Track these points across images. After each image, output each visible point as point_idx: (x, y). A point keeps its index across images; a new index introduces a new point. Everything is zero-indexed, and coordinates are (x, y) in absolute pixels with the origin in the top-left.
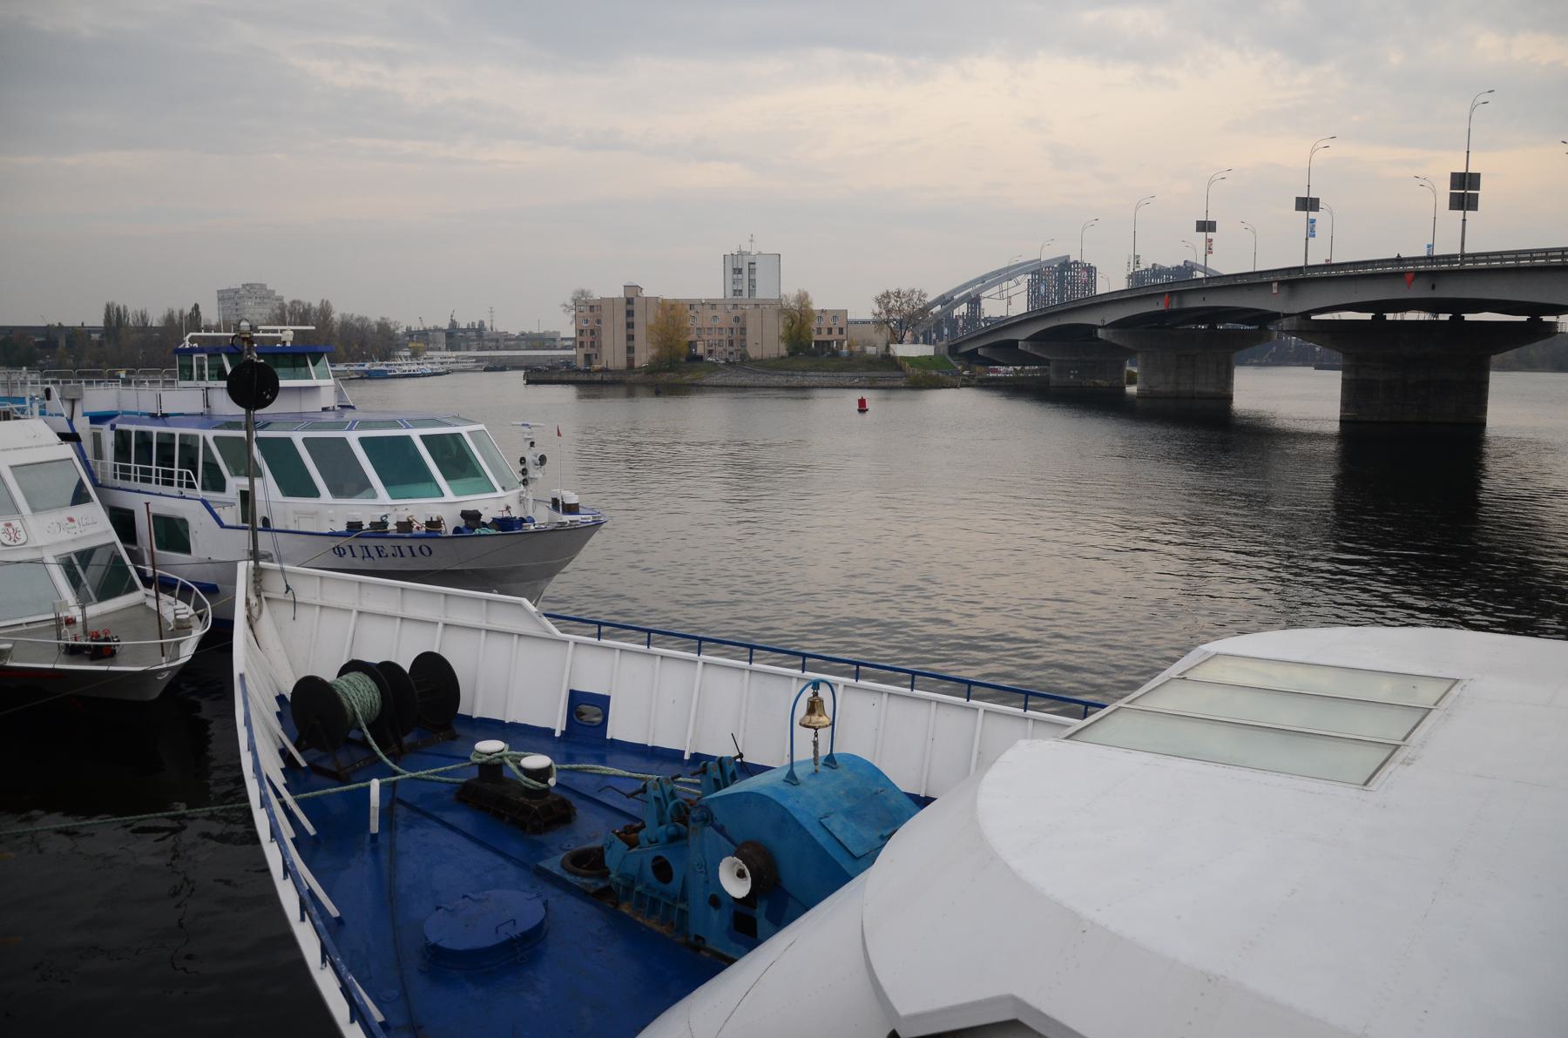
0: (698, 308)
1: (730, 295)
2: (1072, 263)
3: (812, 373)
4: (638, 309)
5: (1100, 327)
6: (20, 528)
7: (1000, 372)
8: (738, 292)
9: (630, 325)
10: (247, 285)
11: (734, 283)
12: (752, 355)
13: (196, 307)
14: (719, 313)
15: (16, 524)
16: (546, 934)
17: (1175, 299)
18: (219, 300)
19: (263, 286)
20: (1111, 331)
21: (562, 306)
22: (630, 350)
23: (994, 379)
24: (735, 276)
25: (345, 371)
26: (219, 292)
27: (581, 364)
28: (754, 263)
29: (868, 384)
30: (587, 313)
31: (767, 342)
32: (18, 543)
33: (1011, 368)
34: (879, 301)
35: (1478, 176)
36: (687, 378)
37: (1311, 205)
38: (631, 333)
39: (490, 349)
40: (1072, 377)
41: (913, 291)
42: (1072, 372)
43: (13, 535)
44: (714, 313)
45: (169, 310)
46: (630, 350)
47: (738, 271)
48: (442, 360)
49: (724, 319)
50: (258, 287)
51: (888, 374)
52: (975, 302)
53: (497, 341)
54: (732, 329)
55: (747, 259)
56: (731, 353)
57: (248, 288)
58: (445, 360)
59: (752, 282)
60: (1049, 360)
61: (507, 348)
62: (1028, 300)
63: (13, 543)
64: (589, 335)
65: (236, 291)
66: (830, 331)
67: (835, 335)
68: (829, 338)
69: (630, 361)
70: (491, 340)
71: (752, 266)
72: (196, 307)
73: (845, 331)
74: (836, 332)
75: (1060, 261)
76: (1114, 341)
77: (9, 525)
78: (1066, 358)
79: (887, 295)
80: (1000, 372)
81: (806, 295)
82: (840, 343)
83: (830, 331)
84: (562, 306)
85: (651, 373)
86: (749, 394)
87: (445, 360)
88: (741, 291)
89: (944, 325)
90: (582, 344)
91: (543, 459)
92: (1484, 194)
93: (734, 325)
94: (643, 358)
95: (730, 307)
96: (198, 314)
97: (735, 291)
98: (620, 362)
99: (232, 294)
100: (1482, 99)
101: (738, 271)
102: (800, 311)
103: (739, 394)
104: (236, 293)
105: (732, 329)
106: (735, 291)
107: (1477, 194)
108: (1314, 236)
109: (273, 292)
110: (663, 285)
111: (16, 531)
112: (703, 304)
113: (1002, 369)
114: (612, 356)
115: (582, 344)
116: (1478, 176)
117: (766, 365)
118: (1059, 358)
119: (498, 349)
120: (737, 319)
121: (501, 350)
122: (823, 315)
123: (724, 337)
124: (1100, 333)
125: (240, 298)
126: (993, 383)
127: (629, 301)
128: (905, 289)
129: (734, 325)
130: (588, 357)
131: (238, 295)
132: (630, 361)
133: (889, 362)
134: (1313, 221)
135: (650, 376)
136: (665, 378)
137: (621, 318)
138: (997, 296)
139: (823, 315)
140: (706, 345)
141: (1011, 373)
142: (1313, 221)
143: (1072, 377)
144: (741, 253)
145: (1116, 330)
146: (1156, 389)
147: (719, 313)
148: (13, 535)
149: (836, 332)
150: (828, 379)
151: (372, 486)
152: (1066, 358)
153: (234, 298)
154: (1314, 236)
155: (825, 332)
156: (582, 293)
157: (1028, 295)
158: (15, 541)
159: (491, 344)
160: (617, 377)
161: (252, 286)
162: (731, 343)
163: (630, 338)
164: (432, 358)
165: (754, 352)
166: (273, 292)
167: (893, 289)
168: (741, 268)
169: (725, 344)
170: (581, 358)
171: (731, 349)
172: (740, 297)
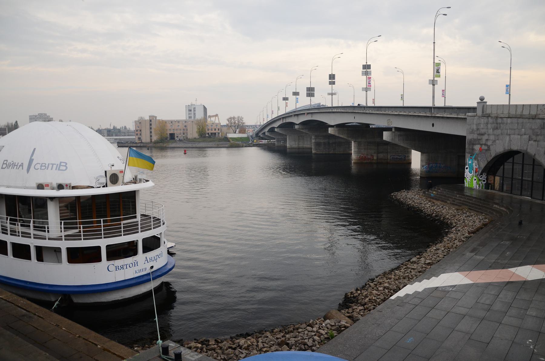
0: (173, 123)
1: (188, 118)
2: (321, 106)
3: (202, 143)
4: (153, 123)
5: (276, 128)
7: (263, 142)
8: (190, 117)
9: (151, 128)
10: (40, 114)
11: (189, 114)
12: (188, 137)
13: (16, 122)
14: (180, 124)
17: (284, 120)
18: (30, 119)
19: (45, 114)
20: (279, 129)
22: (151, 136)
23: (261, 144)
24: (189, 112)
26: (30, 116)
27: (137, 141)
29: (216, 146)
30: (139, 124)
31: (193, 133)
33: (266, 141)
34: (228, 120)
35: (314, 88)
36: (165, 145)
37: (297, 94)
39: (123, 136)
40: (282, 143)
41: (239, 117)
44: (179, 124)
45: (7, 123)
46: (151, 136)
47: (190, 110)
49: (181, 126)
50: (43, 115)
51: (225, 143)
53: (125, 133)
54: (184, 129)
55: (193, 107)
56: (184, 137)
57: (40, 115)
59: (194, 114)
60: (275, 138)
61: (128, 136)
64: (138, 132)
65: (36, 116)
66: (215, 130)
67: (217, 131)
68: (215, 132)
69: (151, 139)
70: (123, 133)
71: (195, 109)
72: (16, 122)
73: (220, 129)
74: (217, 130)
75: (318, 105)
76: (280, 132)
78: (280, 137)
79: (231, 118)
80: (263, 142)
82: (219, 133)
83: (215, 130)
85: (155, 143)
86: (176, 149)
88: (191, 117)
90: (137, 134)
91: (12, 161)
92: (316, 93)
93: (184, 128)
94: (155, 138)
95: (184, 122)
96: (17, 124)
97: (189, 117)
98: (148, 140)
99: (35, 117)
100: (314, 68)
101: (190, 110)
102: (8, 125)
104: (36, 116)
105: (184, 129)
106: (189, 117)
107: (314, 93)
108: (298, 102)
109: (49, 116)
110: (162, 116)
112: (175, 121)
113: (264, 141)
114: (146, 138)
115: (137, 134)
116: (314, 88)
117: (194, 140)
118: (277, 137)
119: (125, 136)
120: (185, 126)
121: (126, 136)
122: (213, 125)
123: (182, 132)
124: (276, 130)
125: (37, 118)
126: (261, 145)
127: (151, 121)
128: (236, 116)
129: (184, 128)
130: (139, 138)
131: (36, 117)
132: (151, 139)
133: (226, 139)
134: (297, 98)
135: (155, 144)
136: (158, 145)
137: (148, 126)
139: (213, 125)
141: (266, 142)
142: (297, 98)
143: (282, 143)
144: (192, 105)
145: (280, 129)
146: (292, 146)
147: (180, 124)
149: (217, 130)
150: (205, 145)
151: (135, 191)
152: (280, 137)
153: (35, 118)
154: (298, 102)
155: (214, 130)
156: (141, 118)
159: (123, 134)
160: (145, 145)
161: (41, 114)
162: (184, 134)
163: (151, 132)
165: (190, 136)
166: (49, 116)
167: (232, 116)
168: (191, 110)
169: (182, 134)
170: (137, 139)
171: (184, 136)
172: (191, 119)
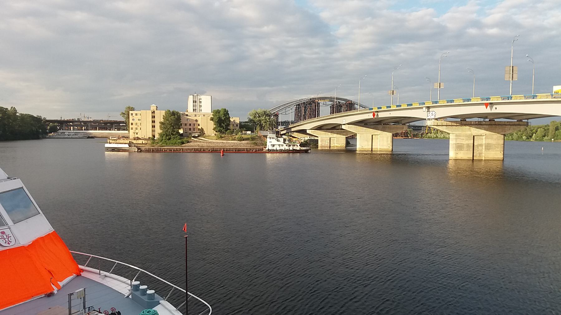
6: (11, 235)
9: (153, 122)
15: (7, 232)
16: (56, 245)
21: (121, 115)
22: (153, 131)
25: (485, 146)
28: (201, 99)
32: (10, 245)
38: (154, 125)
42: (327, 141)
43: (7, 240)
48: (69, 134)
52: (276, 116)
58: (70, 134)
62: (319, 114)
63: (8, 245)
71: (200, 100)
77: (3, 233)
81: (225, 110)
84: (121, 115)
87: (70, 134)
89: (38, 130)
103: (436, 159)
111: (8, 237)
138: (284, 113)
140: (184, 130)
148: (7, 240)
149: (188, 125)
157: (295, 113)
158: (9, 243)
164: (64, 133)
